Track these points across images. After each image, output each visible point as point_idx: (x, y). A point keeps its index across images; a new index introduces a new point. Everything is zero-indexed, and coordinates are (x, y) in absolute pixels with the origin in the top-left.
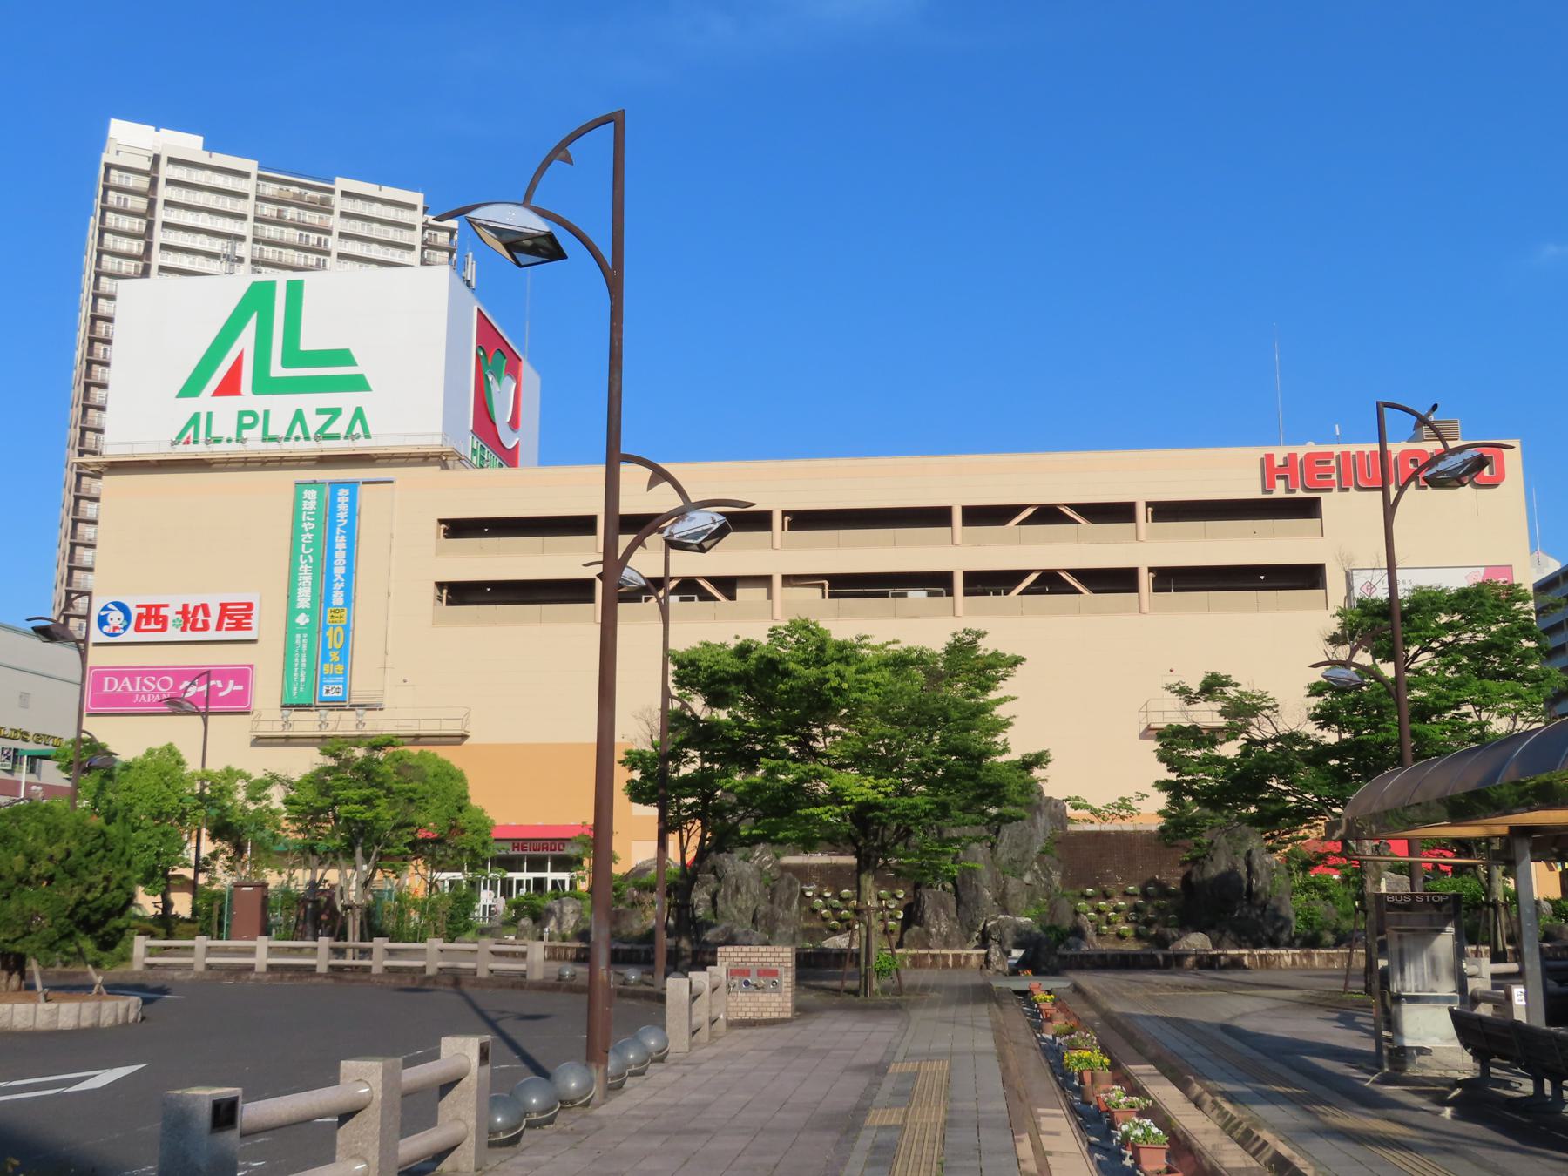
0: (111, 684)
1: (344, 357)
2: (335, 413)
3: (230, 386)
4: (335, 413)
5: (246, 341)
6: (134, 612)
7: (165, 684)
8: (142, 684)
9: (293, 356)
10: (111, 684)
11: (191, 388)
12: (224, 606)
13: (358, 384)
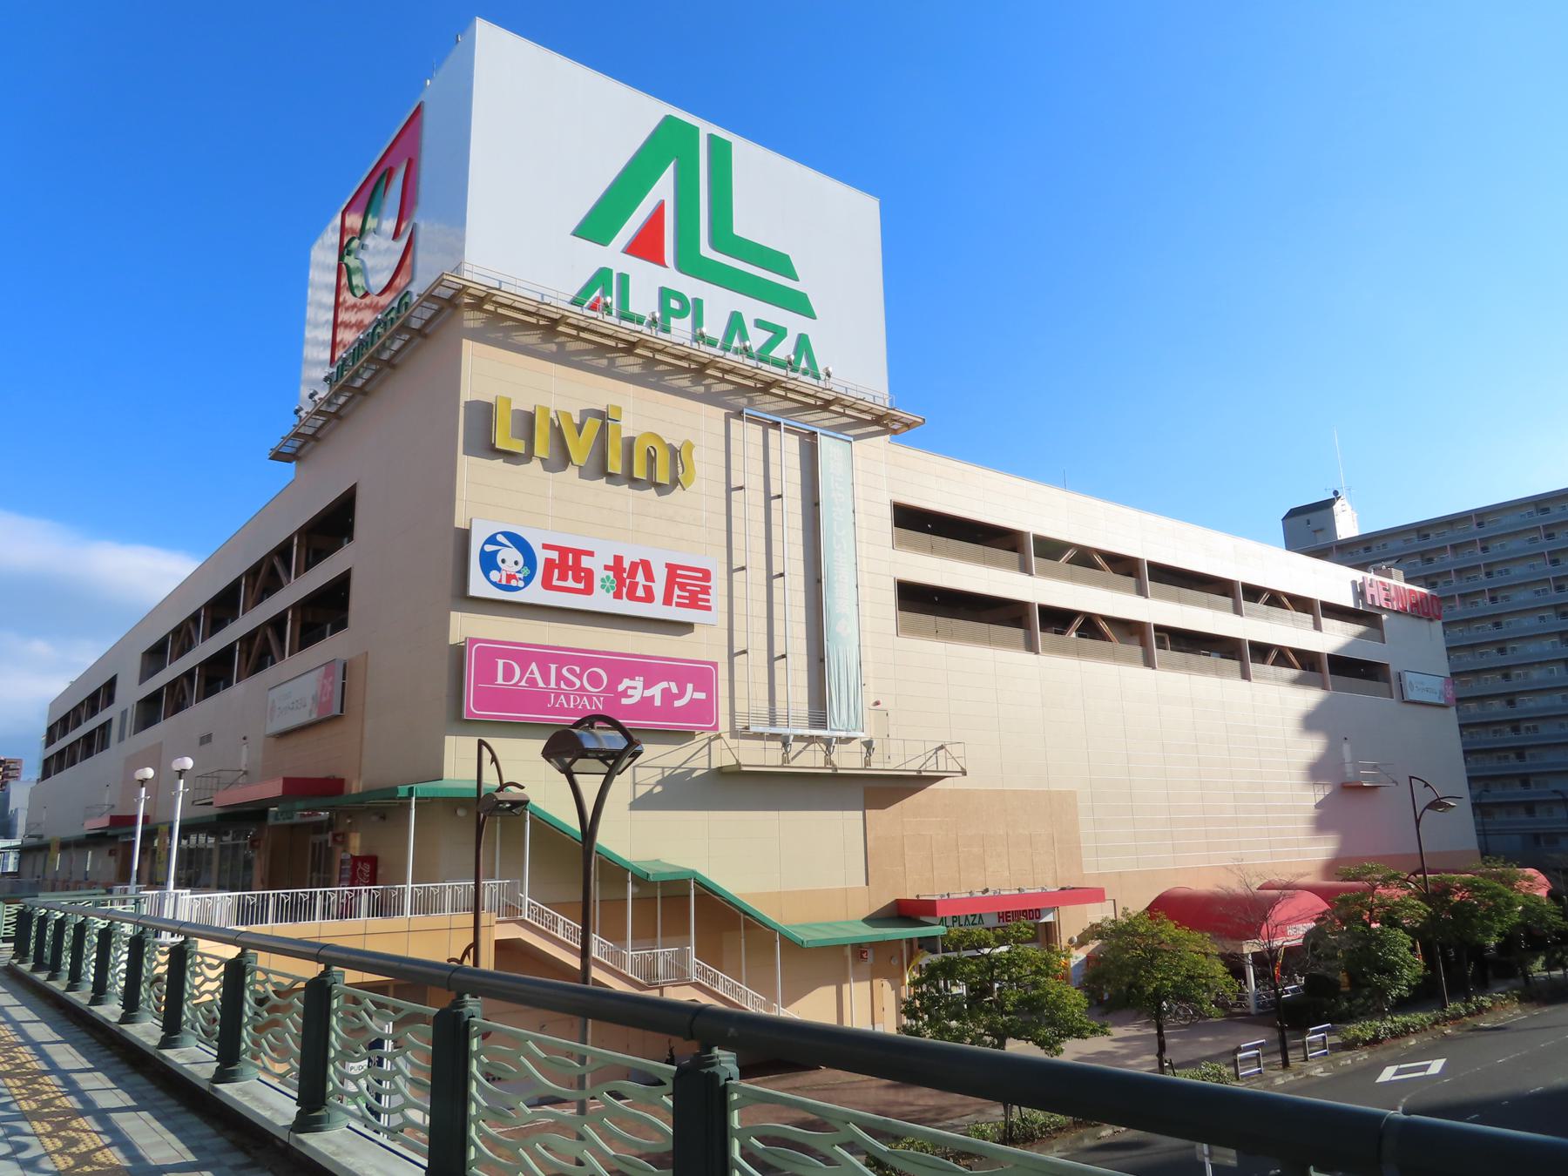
0: (509, 674)
1: (782, 264)
2: (778, 333)
3: (647, 246)
4: (778, 333)
5: (663, 189)
6: (541, 556)
7: (595, 680)
8: (560, 677)
9: (723, 237)
10: (509, 674)
11: (595, 227)
12: (672, 569)
13: (799, 304)
